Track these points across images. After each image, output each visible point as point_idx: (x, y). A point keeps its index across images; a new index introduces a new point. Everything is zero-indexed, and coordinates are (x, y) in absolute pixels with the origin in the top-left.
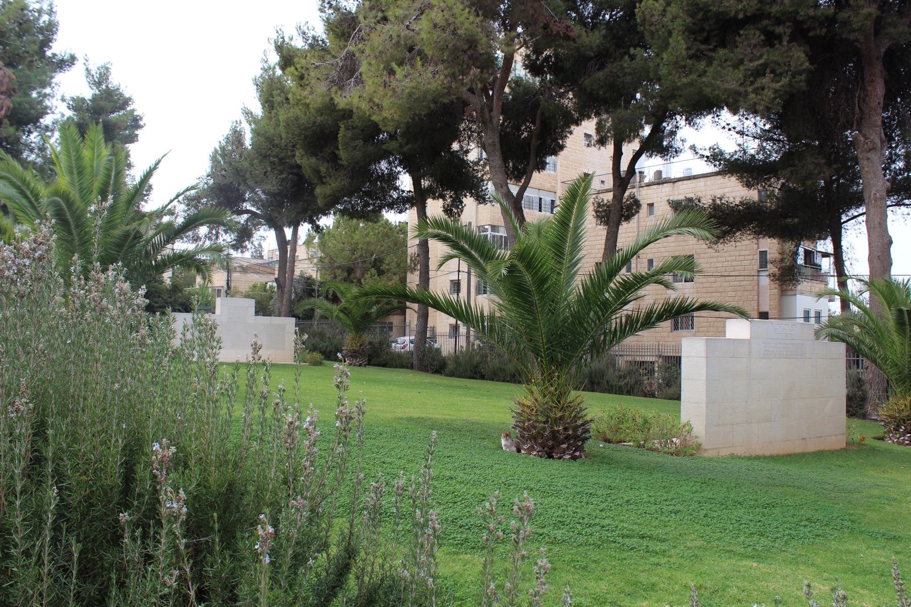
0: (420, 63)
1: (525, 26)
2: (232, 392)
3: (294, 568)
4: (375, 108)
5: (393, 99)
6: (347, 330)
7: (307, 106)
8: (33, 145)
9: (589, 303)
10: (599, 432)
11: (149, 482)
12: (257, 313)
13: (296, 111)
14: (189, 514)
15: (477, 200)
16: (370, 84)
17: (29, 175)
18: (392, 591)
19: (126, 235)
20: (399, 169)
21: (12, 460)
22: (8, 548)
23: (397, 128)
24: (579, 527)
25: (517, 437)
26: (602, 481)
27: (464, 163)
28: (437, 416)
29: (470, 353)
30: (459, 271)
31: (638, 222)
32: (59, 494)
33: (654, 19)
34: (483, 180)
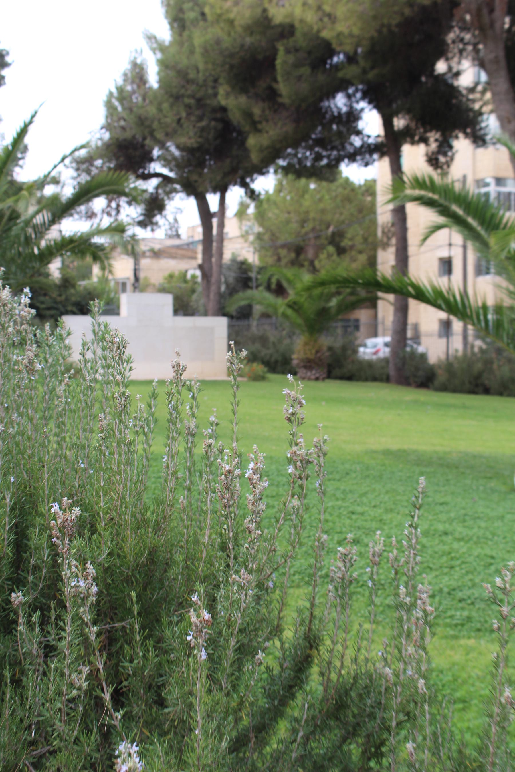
2: (149, 428)
3: (238, 664)
4: (326, 19)
6: (297, 331)
7: (231, 22)
11: (47, 552)
12: (176, 312)
14: (99, 594)
18: (369, 692)
20: (362, 104)
23: (357, 46)
27: (454, 91)
30: (450, 245)
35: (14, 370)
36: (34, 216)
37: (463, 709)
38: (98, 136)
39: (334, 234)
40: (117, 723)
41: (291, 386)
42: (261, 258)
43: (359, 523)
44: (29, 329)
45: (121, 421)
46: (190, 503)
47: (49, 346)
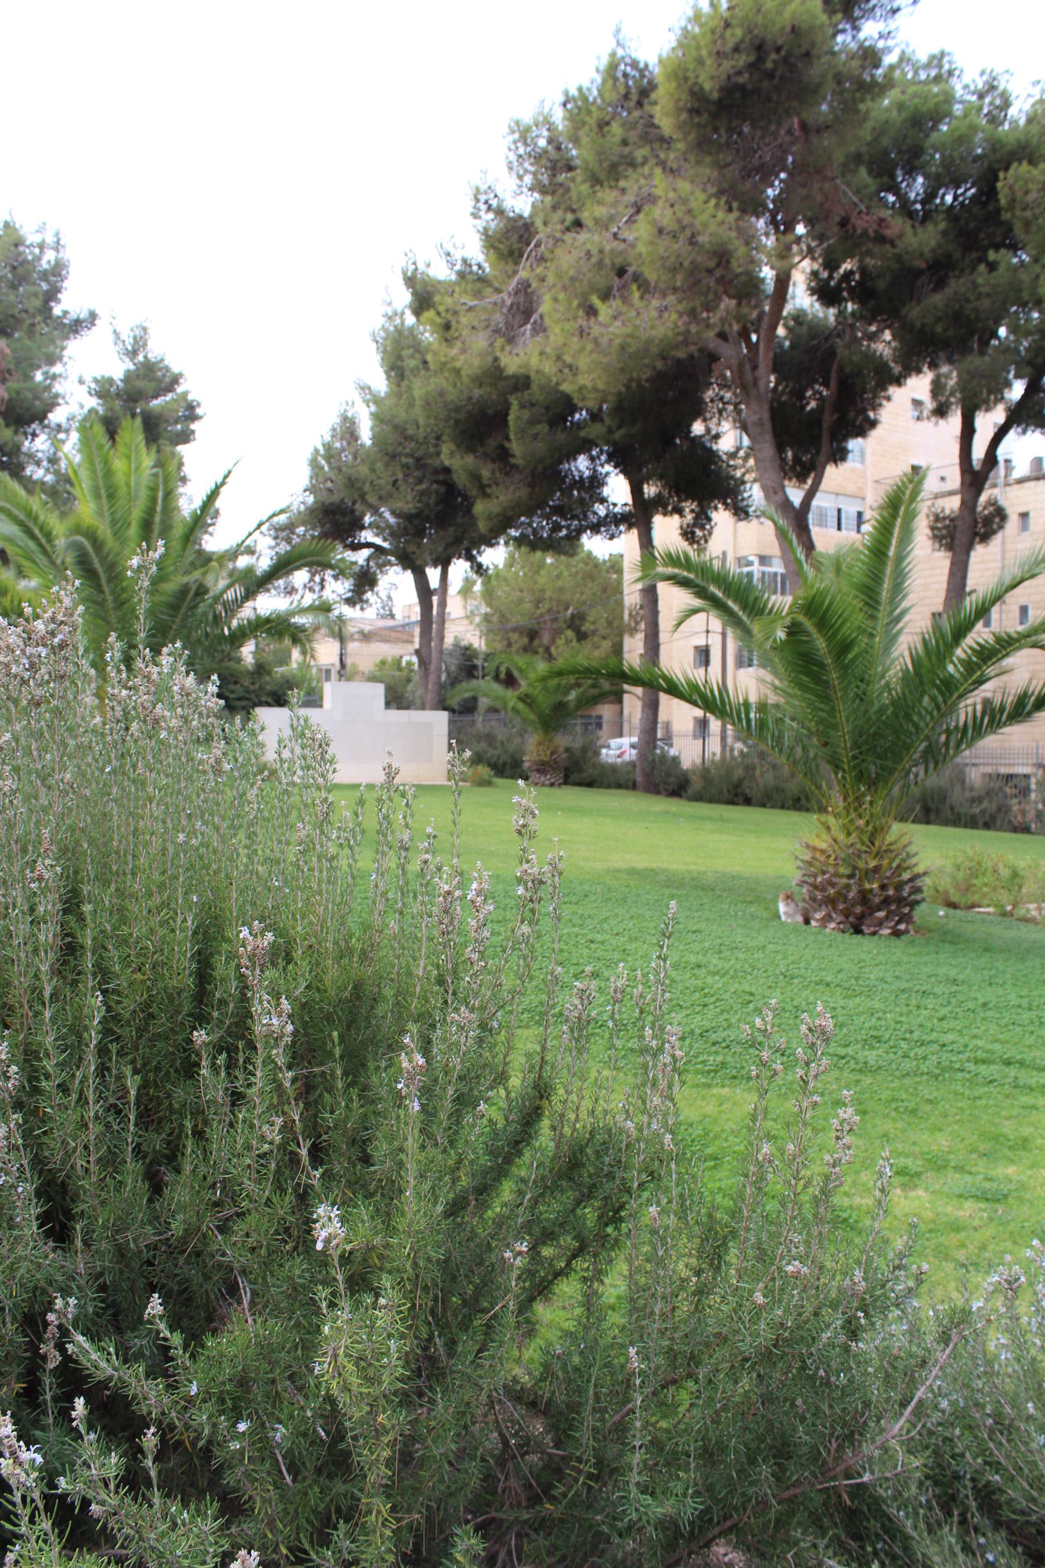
0: (637, 295)
1: (810, 222)
3: (456, 1116)
4: (566, 371)
5: (594, 356)
6: (530, 729)
7: (457, 372)
8: (40, 455)
9: (921, 683)
10: (937, 891)
11: (234, 984)
12: (388, 705)
13: (440, 382)
14: (295, 1033)
15: (735, 514)
16: (556, 333)
17: (35, 503)
18: (607, 1149)
19: (184, 591)
20: (608, 468)
21: (36, 951)
22: (38, 1080)
23: (602, 401)
24: (904, 1045)
25: (804, 900)
26: (942, 971)
27: (712, 456)
28: (675, 867)
29: (726, 765)
30: (708, 632)
31: (1003, 543)
32: (105, 1003)
33: (1030, 198)
34: (743, 483)
35: (198, 771)
36: (224, 591)
37: (714, 1167)
38: (301, 499)
39: (573, 616)
40: (315, 1182)
41: (522, 793)
42: (488, 643)
43: (600, 953)
44: (216, 722)
45: (322, 832)
46: (402, 928)
47: (240, 744)
